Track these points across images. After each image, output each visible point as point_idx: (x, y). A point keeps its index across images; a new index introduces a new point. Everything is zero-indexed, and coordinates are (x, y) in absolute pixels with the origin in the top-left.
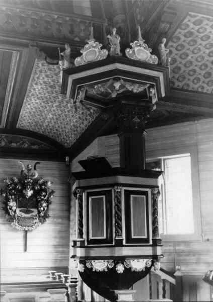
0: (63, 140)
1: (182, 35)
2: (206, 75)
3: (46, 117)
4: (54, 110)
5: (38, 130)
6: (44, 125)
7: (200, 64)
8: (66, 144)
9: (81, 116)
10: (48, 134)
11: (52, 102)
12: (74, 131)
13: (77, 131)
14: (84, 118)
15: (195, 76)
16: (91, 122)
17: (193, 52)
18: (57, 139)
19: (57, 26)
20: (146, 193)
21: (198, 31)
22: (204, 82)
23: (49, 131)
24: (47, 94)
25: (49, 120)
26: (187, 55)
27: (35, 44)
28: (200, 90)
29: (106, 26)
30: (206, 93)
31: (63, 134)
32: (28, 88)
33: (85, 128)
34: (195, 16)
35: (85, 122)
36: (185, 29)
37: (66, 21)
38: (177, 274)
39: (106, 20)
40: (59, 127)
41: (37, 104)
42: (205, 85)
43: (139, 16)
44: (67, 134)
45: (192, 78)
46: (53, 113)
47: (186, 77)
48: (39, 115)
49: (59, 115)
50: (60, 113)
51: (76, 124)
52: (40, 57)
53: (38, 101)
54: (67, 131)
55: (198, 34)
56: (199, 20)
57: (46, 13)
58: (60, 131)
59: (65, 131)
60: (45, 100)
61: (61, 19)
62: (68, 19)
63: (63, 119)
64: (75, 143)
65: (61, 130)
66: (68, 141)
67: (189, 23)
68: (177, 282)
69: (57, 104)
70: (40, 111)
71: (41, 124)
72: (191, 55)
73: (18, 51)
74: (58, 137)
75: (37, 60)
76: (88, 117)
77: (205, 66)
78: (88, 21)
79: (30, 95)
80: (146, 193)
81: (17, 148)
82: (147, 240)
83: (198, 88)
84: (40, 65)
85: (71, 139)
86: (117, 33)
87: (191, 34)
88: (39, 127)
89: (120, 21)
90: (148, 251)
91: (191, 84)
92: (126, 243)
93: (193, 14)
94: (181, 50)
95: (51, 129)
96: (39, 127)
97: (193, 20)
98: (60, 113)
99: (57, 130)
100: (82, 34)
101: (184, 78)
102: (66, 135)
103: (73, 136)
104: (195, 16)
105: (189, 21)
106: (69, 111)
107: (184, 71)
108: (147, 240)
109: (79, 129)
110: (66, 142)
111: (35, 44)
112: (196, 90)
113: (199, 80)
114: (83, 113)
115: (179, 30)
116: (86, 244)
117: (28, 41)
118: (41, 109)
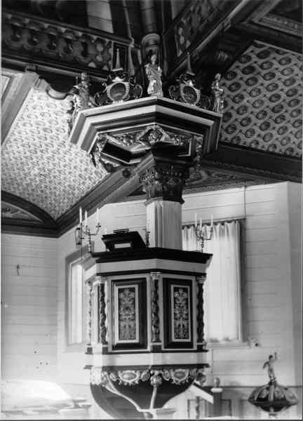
0: (49, 206)
1: (240, 69)
2: (263, 127)
3: (29, 173)
4: (43, 164)
5: (12, 190)
6: (24, 183)
7: (257, 111)
8: (53, 212)
9: (83, 173)
10: (27, 196)
11: (42, 151)
12: (69, 194)
13: (73, 194)
14: (87, 177)
15: (249, 127)
16: (97, 183)
17: (250, 94)
18: (41, 204)
19: (65, 45)
20: (189, 283)
21: (261, 66)
22: (259, 136)
23: (30, 192)
24: (37, 140)
25: (33, 177)
26: (242, 97)
27: (34, 68)
28: (253, 146)
29: (132, 48)
30: (279, 155)
31: (50, 198)
32: (12, 129)
33: (86, 191)
34: (261, 46)
35: (88, 182)
36: (245, 63)
37: (78, 38)
38: (222, 384)
39: (133, 40)
40: (46, 187)
41: (19, 153)
42: (261, 140)
43: (182, 39)
44: (58, 198)
45: (244, 129)
46: (41, 166)
47: (237, 127)
48: (18, 169)
49: (50, 171)
50: (51, 167)
51: (72, 183)
52: (37, 85)
53: (21, 148)
54: (57, 193)
55: (260, 70)
56: (266, 51)
57: (31, 18)
58: (47, 194)
59: (55, 193)
60: (32, 148)
61: (70, 34)
62: (80, 34)
63: (55, 177)
64: (67, 211)
65: (48, 191)
66: (57, 208)
67: (251, 54)
68: (215, 399)
69: (50, 155)
70: (22, 163)
71: (20, 181)
72: (247, 98)
73: (7, 76)
74: (42, 201)
75: (32, 90)
76: (94, 175)
77: (281, 118)
78: (107, 40)
79: (12, 140)
80: (189, 283)
81: (13, 219)
82: (190, 345)
83: (232, 139)
84: (35, 98)
85: (62, 204)
86: (157, 63)
87: (252, 69)
88: (16, 186)
89: (151, 42)
90: (191, 358)
91: (242, 136)
92: (165, 348)
93: (259, 42)
94: (235, 90)
95: (33, 190)
96: (16, 186)
97: (258, 51)
98: (51, 167)
99: (42, 191)
100: (99, 58)
101: (235, 128)
102: (54, 199)
103: (66, 201)
104: (261, 46)
105: (252, 52)
106: (65, 166)
107: (236, 120)
108: (190, 345)
109: (76, 192)
110: (54, 210)
111: (34, 68)
112: (247, 145)
113: (253, 132)
114: (86, 170)
115: (237, 63)
116: (110, 350)
117: (24, 63)
118: (24, 160)
